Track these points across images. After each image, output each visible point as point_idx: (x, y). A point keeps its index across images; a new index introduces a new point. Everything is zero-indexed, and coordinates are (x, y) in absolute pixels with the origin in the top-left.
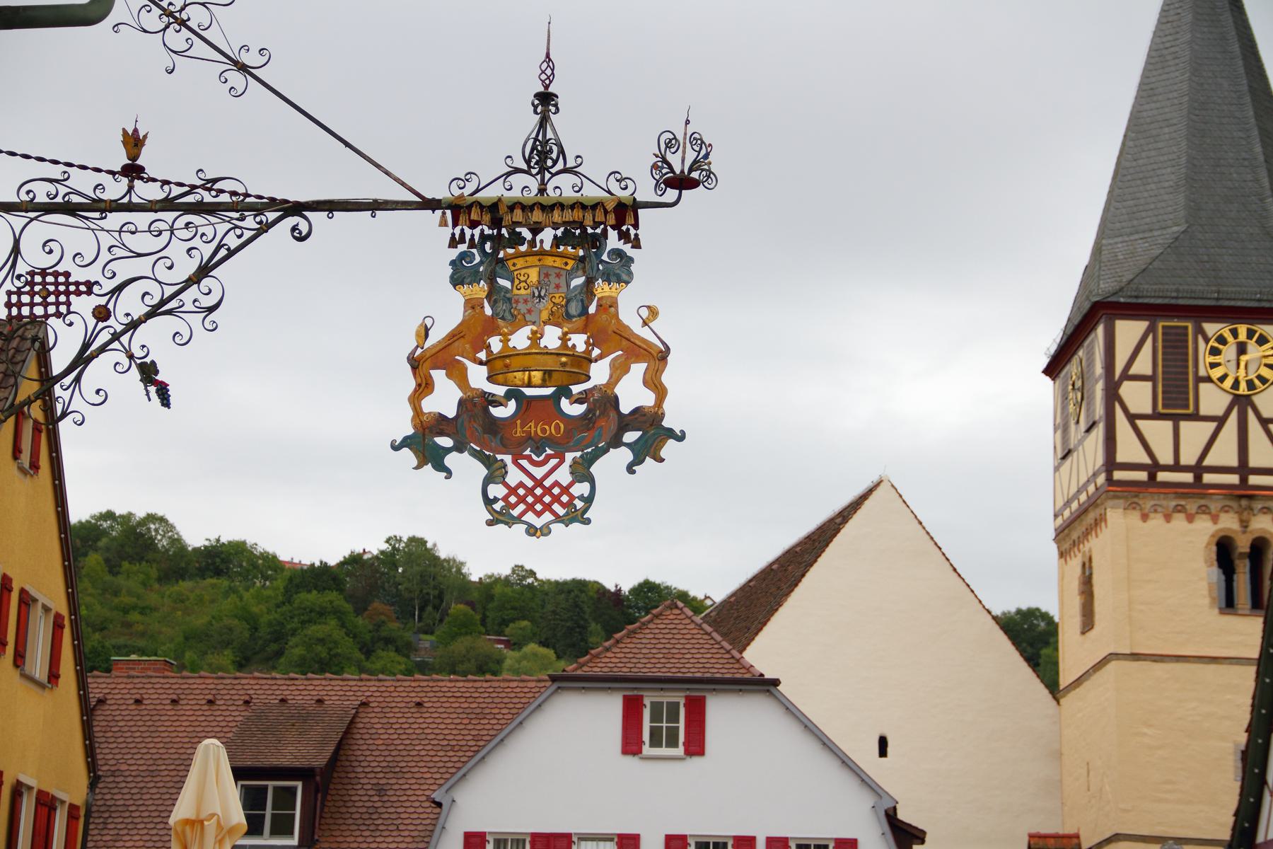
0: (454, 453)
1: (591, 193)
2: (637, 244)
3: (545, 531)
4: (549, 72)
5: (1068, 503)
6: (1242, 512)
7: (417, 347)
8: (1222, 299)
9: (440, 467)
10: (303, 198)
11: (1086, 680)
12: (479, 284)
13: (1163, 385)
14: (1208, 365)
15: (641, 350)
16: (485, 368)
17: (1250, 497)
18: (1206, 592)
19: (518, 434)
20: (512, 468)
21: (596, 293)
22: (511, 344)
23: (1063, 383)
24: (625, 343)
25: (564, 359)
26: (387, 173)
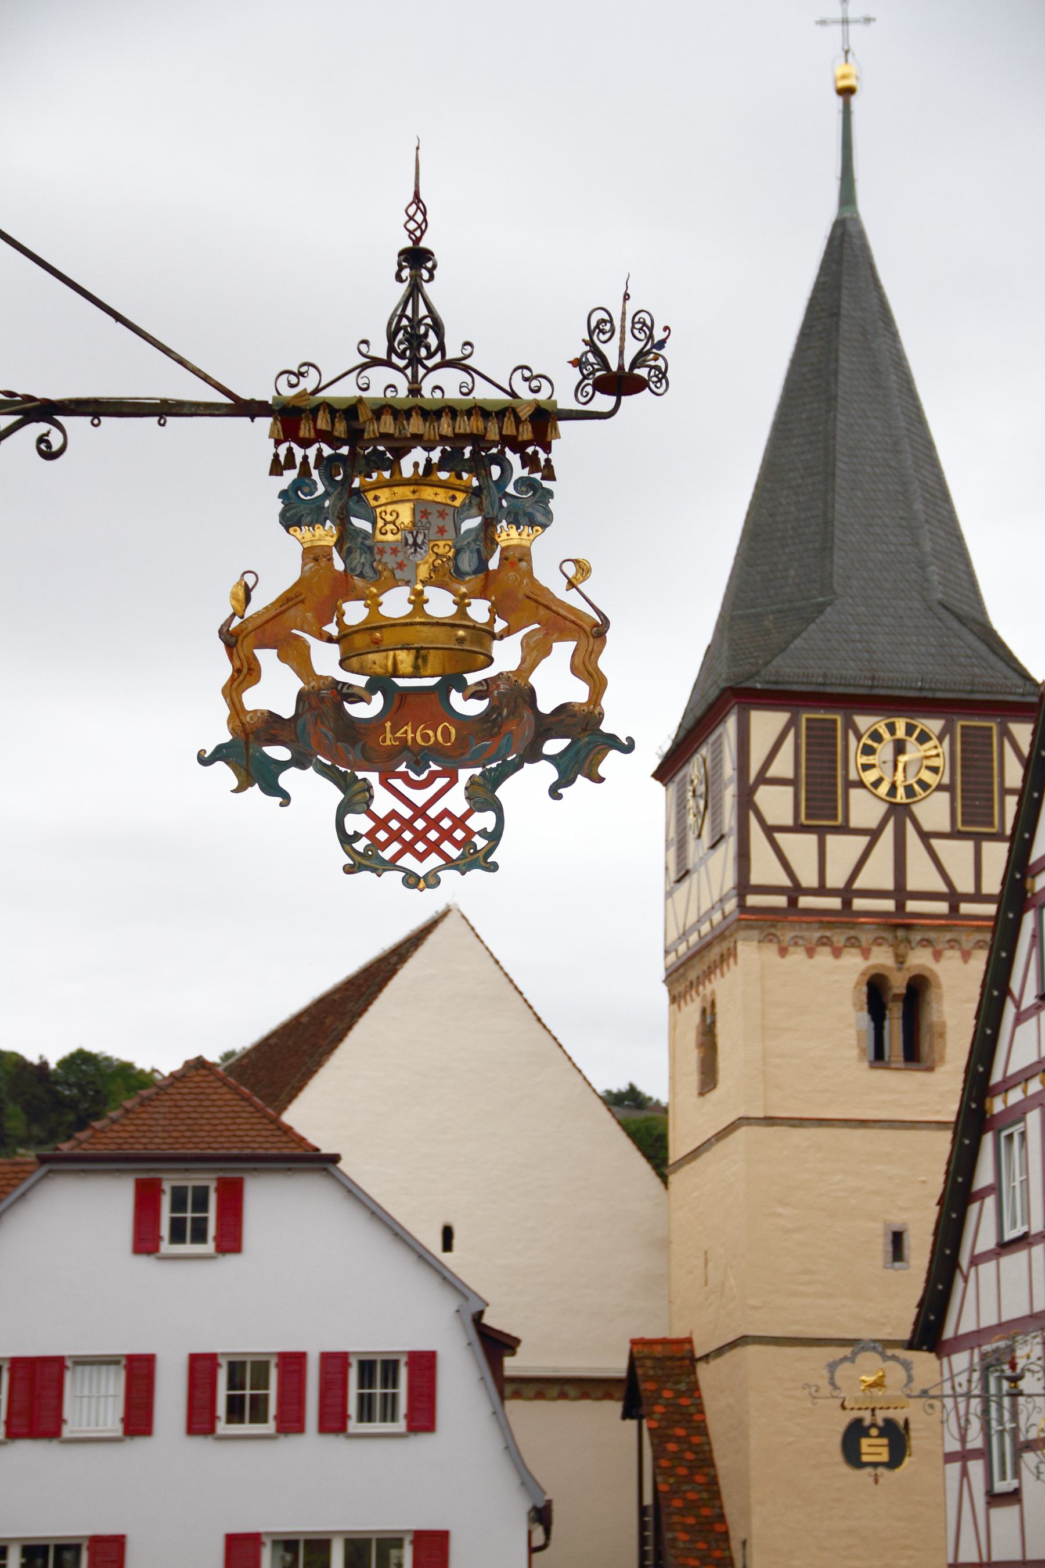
0: (293, 771)
1: (484, 392)
2: (550, 475)
3: (432, 881)
4: (419, 217)
5: (684, 936)
6: (898, 945)
7: (234, 615)
8: (877, 687)
9: (272, 788)
10: (55, 395)
11: (706, 1150)
12: (324, 525)
13: (807, 792)
14: (859, 766)
15: (568, 623)
16: (335, 648)
17: (908, 927)
18: (854, 1042)
19: (388, 743)
20: (379, 790)
21: (499, 540)
22: (382, 610)
23: (678, 791)
24: (542, 612)
25: (461, 633)
26: (181, 362)
